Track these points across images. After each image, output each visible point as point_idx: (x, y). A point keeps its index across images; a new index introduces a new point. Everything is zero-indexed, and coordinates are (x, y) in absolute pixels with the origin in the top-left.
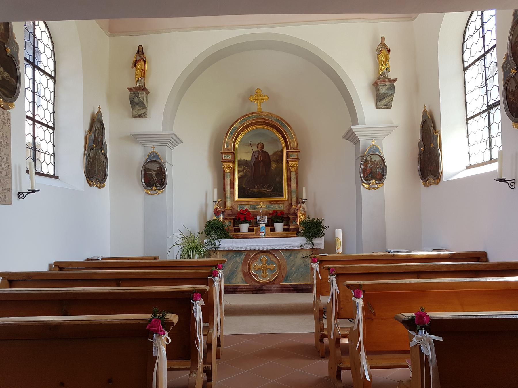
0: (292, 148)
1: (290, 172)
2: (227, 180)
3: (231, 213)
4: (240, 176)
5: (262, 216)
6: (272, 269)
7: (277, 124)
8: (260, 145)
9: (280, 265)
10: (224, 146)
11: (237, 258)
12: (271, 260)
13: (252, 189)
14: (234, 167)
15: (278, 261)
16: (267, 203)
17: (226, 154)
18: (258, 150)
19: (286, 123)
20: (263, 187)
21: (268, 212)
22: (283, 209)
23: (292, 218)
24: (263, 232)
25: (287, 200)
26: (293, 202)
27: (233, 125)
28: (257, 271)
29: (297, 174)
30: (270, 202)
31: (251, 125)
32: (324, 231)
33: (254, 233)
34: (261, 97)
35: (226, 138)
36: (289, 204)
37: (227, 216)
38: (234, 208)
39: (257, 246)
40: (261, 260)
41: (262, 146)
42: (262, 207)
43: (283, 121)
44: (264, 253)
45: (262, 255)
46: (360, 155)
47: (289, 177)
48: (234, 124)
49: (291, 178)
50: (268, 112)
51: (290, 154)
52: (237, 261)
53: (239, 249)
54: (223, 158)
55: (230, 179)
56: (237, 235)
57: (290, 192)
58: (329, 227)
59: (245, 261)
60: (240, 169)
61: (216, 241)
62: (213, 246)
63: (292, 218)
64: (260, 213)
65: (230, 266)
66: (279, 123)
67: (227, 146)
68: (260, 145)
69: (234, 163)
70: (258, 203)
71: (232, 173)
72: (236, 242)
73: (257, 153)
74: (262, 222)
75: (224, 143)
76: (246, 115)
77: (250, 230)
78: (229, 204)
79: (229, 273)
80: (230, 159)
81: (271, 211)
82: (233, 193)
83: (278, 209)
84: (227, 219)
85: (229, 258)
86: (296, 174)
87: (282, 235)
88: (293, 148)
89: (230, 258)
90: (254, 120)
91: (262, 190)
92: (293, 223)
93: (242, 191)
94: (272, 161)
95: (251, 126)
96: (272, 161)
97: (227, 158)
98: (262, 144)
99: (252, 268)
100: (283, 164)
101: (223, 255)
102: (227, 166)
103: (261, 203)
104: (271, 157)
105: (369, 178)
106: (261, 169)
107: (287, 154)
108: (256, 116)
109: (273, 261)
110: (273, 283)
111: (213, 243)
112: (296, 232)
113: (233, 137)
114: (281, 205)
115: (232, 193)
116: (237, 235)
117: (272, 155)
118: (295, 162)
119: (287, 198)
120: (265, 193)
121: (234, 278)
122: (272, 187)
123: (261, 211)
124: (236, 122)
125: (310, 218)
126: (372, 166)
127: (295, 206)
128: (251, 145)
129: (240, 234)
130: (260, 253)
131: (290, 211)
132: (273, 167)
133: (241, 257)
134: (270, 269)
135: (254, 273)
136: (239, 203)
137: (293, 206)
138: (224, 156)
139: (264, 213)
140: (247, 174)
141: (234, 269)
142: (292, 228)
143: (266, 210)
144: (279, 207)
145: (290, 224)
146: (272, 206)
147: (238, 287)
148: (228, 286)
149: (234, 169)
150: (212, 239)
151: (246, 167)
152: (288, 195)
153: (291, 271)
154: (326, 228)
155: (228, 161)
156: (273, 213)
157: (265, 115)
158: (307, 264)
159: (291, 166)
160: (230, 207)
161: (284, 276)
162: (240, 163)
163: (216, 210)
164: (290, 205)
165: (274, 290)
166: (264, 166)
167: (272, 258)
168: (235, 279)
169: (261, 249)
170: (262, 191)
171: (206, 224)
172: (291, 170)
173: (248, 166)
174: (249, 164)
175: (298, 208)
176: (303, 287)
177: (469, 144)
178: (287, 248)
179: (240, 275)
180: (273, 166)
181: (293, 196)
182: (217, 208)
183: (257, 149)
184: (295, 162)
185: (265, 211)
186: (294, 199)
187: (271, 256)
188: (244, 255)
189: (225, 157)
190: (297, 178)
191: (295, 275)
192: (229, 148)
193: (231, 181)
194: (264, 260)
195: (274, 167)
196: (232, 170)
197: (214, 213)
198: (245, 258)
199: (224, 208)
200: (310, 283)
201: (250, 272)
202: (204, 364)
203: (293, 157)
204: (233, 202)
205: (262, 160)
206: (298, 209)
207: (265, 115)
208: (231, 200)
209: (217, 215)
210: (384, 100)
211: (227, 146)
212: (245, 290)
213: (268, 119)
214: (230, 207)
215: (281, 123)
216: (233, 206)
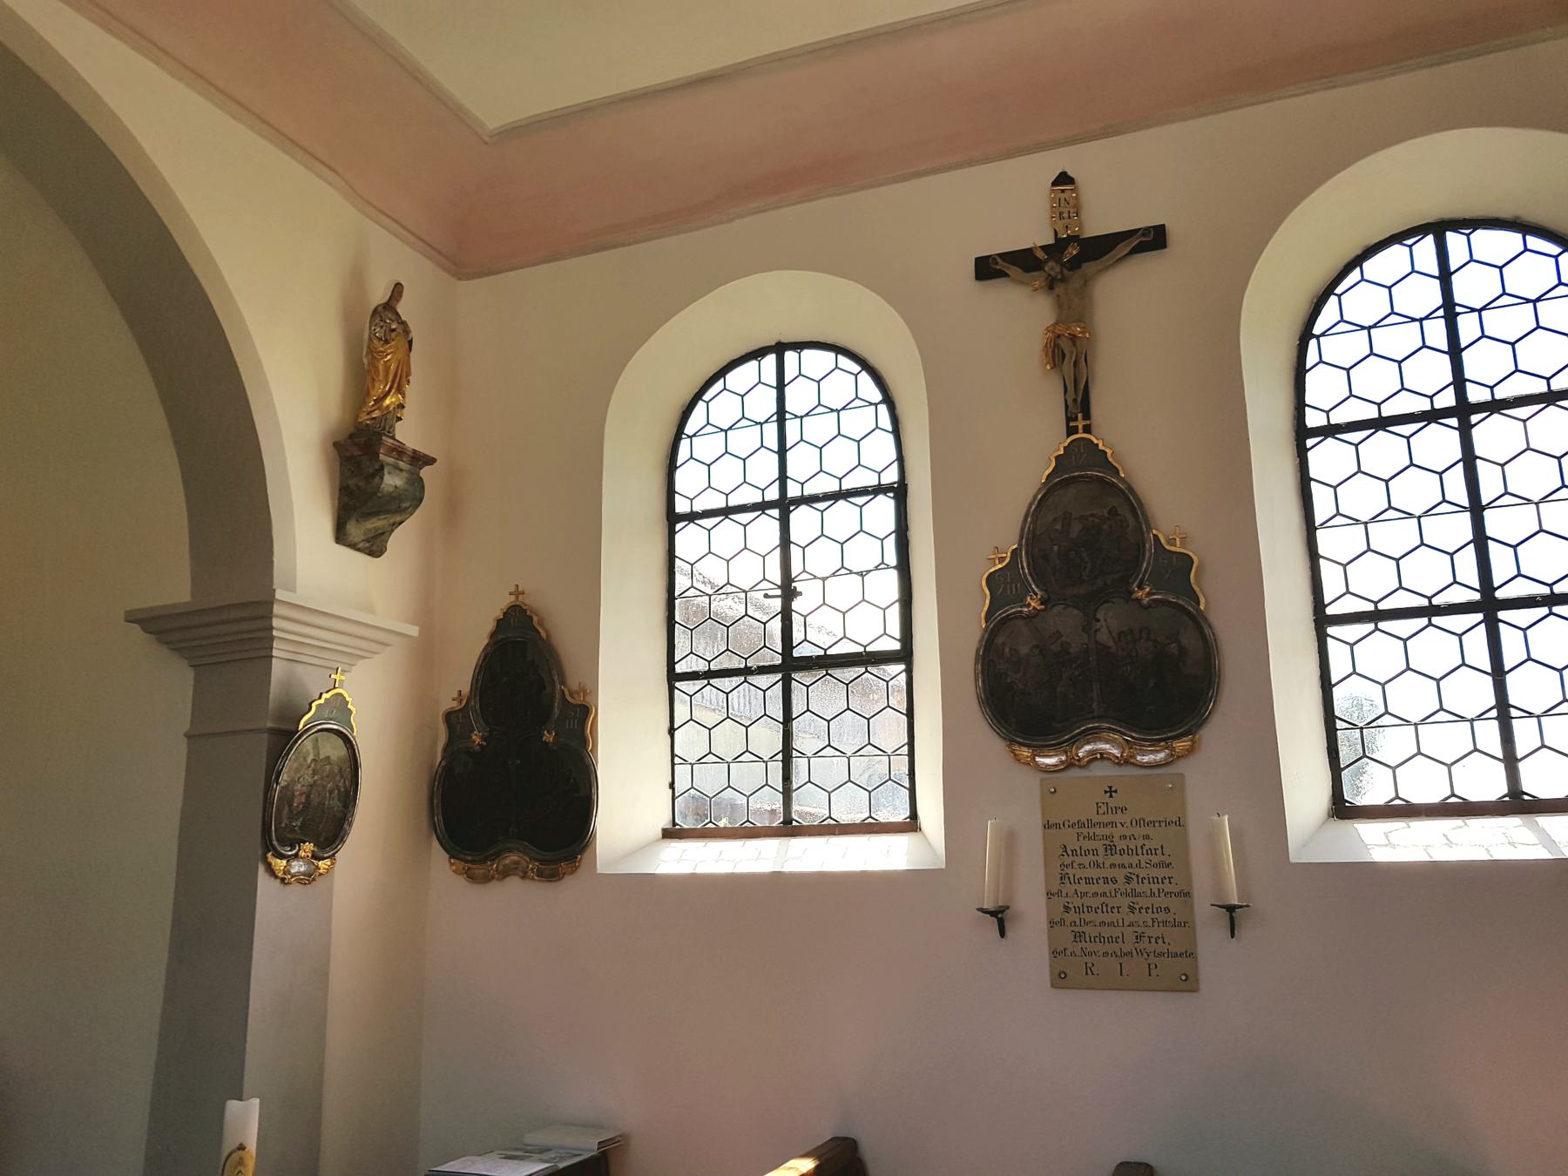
46: (269, 724)
105: (293, 830)
126: (316, 778)
177: (673, 755)
202: (916, 831)
210: (373, 520)
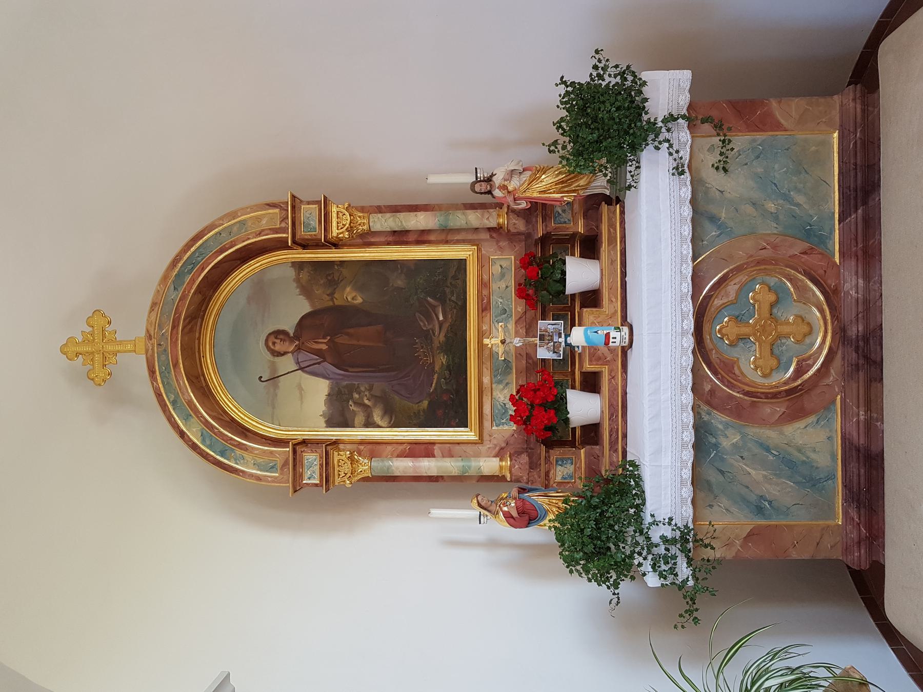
0: (283, 225)
1: (370, 233)
2: (397, 468)
3: (524, 458)
4: (387, 419)
5: (537, 340)
6: (772, 297)
7: (193, 281)
8: (274, 343)
9: (759, 263)
10: (273, 482)
11: (725, 443)
12: (732, 303)
13: (436, 376)
14: (352, 442)
15: (739, 269)
16: (487, 319)
17: (301, 475)
18: (292, 352)
19: (189, 249)
20: (427, 336)
21: (520, 318)
22: (508, 263)
23: (546, 226)
24: (608, 335)
25: (477, 245)
26: (486, 221)
27: (194, 447)
28: (779, 363)
29: (380, 210)
30: (484, 308)
31: (202, 378)
32: (616, 66)
33: (605, 370)
34: (94, 339)
35: (243, 472)
36: (491, 237)
37: (535, 474)
38: (503, 445)
39: (678, 362)
40: (732, 345)
41: (276, 338)
42: (501, 337)
43: (181, 259)
44: (706, 328)
45: (711, 339)
47: (390, 239)
48: (191, 440)
49: (395, 232)
50: (147, 314)
51: (302, 233)
52: (734, 445)
53: (689, 436)
54: (316, 485)
55: (395, 459)
56: (613, 439)
57: (447, 235)
58: (597, 52)
59: (738, 412)
60: (360, 418)
61: (655, 535)
62: (674, 550)
63: (546, 226)
64: (525, 345)
65: (757, 474)
66: (190, 272)
67: (272, 469)
68: (274, 343)
69: (335, 443)
70: (486, 353)
71: (373, 448)
72: (658, 452)
73: (304, 356)
74: (562, 340)
75: (258, 478)
76: (159, 395)
77: (591, 384)
78: (490, 465)
79: (790, 478)
80: (321, 458)
81: (516, 308)
82: (450, 449)
83: (511, 282)
84: (547, 474)
85: (721, 478)
86: (380, 212)
87: (613, 262)
88: (280, 224)
89: (722, 472)
90: (176, 365)
91: (440, 337)
92: (565, 222)
93: (440, 412)
94: (332, 300)
95: (204, 375)
96: (331, 304)
97: (318, 467)
98: (272, 339)
99: (766, 382)
100: (342, 263)
101: (711, 506)
102: (347, 468)
103: (486, 341)
104: (319, 306)
106: (361, 343)
107: (305, 245)
108: (163, 357)
109: (738, 293)
110: (836, 291)
111: (661, 550)
112: (605, 207)
113: (239, 446)
114: (496, 269)
115: (450, 450)
116: (613, 439)
117: (312, 305)
118: (334, 215)
119: (469, 247)
120: (451, 326)
121: (808, 458)
122: (428, 302)
123: (517, 342)
124: (182, 434)
125: (556, 141)
127: (499, 215)
128: (274, 378)
129: (610, 425)
130: (704, 348)
131: (519, 234)
132: (353, 299)
133: (720, 426)
134: (772, 306)
135: (792, 369)
136: (487, 424)
137: (498, 224)
138: (309, 478)
139: (523, 331)
140: (378, 394)
141: (771, 457)
142: (585, 225)
143: (511, 326)
144: (503, 275)
145: (570, 232)
146: (497, 301)
147: (851, 444)
148: (845, 486)
149: (362, 442)
150: (644, 553)
151: (352, 398)
152: (458, 242)
153: (781, 217)
154: (603, 62)
155: (327, 465)
156: (528, 295)
157: (161, 327)
158: (754, 149)
159: (350, 230)
160: (501, 460)
161: (806, 245)
162: (339, 418)
163: (512, 517)
164: (494, 235)
165: (867, 289)
166: (351, 331)
167: (727, 295)
168: (813, 456)
169: (689, 342)
170: (442, 338)
171: (580, 575)
172: (365, 227)
173: (351, 389)
174: (344, 387)
175: (510, 199)
176: (856, 164)
178: (687, 230)
179: (799, 431)
180: (349, 299)
181: (463, 222)
182: (505, 513)
183: (290, 355)
184: (334, 215)
185: (516, 326)
186: (474, 218)
187: (717, 302)
188: (709, 414)
189: (312, 474)
190: (395, 209)
191: (800, 199)
192: (279, 461)
193: (402, 455)
194: (734, 331)
195: (354, 294)
196: (362, 447)
197: (527, 527)
198: (722, 410)
199: (506, 481)
200: (836, 135)
201: (786, 391)
203: (314, 223)
204: (483, 448)
205: (329, 338)
206: (515, 199)
207: (161, 327)
208: (475, 456)
209: (533, 514)
211: (272, 467)
212: (866, 412)
213: (175, 314)
214: (501, 460)
215: (190, 267)
216: (497, 448)
